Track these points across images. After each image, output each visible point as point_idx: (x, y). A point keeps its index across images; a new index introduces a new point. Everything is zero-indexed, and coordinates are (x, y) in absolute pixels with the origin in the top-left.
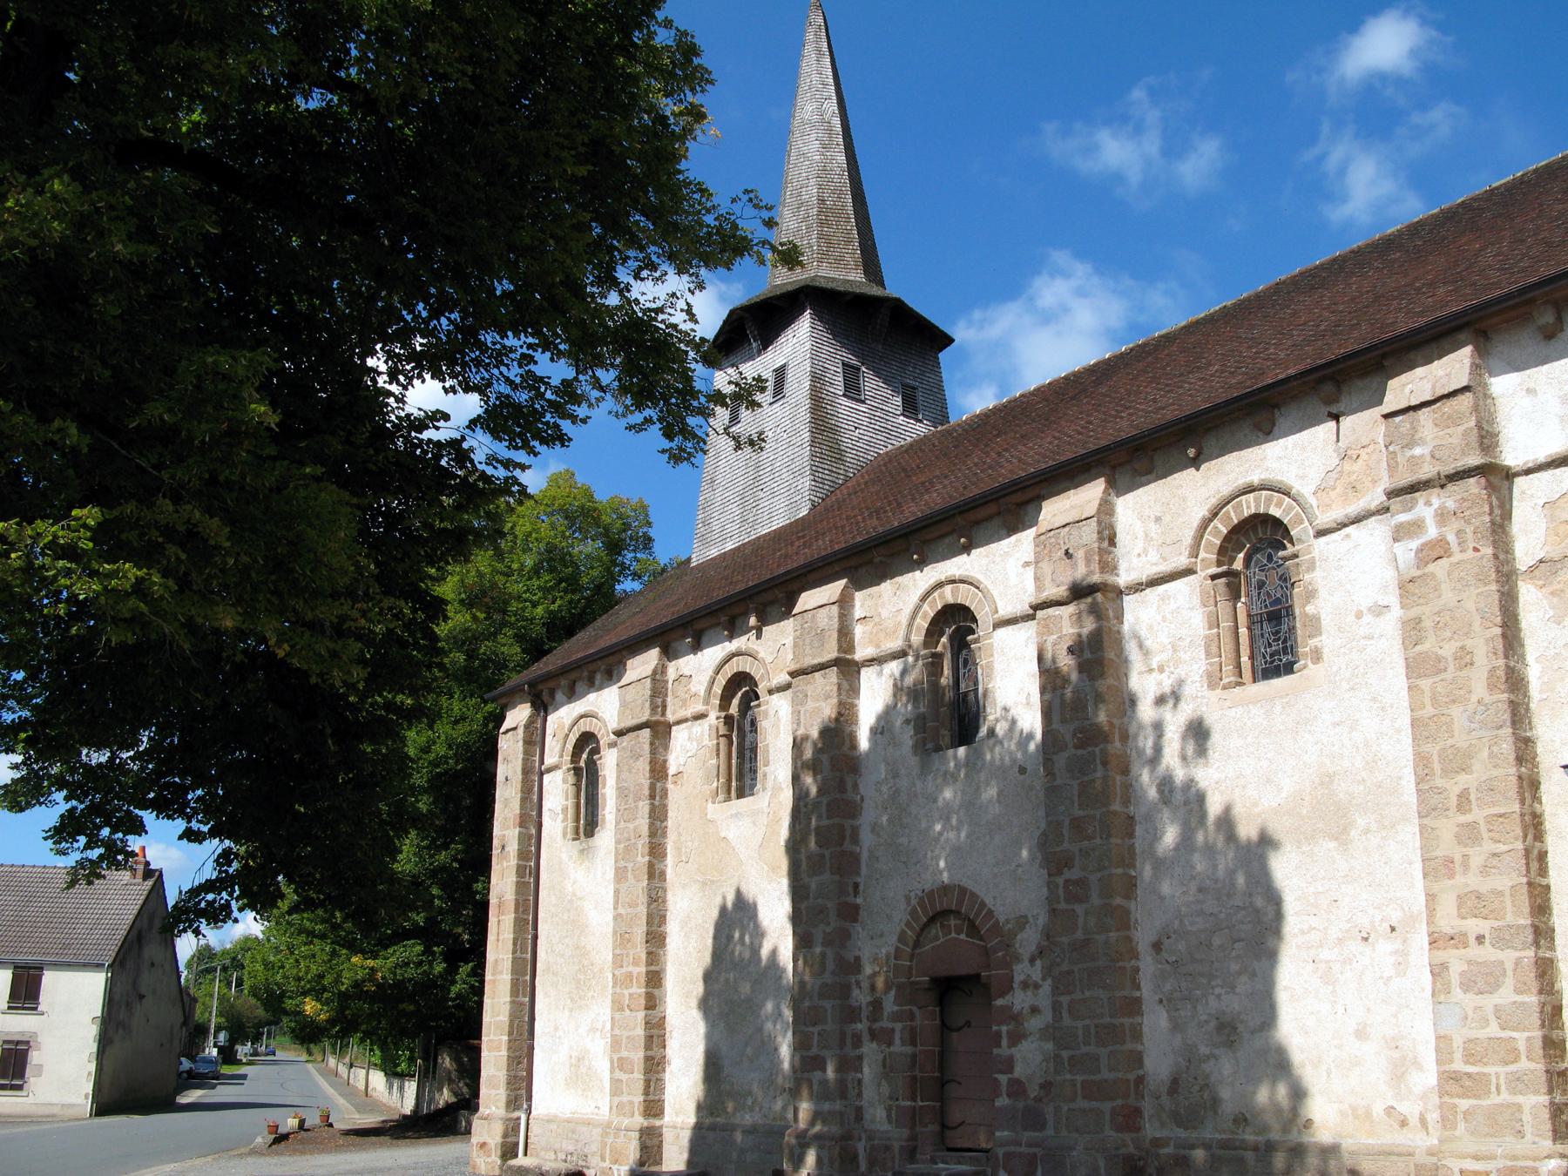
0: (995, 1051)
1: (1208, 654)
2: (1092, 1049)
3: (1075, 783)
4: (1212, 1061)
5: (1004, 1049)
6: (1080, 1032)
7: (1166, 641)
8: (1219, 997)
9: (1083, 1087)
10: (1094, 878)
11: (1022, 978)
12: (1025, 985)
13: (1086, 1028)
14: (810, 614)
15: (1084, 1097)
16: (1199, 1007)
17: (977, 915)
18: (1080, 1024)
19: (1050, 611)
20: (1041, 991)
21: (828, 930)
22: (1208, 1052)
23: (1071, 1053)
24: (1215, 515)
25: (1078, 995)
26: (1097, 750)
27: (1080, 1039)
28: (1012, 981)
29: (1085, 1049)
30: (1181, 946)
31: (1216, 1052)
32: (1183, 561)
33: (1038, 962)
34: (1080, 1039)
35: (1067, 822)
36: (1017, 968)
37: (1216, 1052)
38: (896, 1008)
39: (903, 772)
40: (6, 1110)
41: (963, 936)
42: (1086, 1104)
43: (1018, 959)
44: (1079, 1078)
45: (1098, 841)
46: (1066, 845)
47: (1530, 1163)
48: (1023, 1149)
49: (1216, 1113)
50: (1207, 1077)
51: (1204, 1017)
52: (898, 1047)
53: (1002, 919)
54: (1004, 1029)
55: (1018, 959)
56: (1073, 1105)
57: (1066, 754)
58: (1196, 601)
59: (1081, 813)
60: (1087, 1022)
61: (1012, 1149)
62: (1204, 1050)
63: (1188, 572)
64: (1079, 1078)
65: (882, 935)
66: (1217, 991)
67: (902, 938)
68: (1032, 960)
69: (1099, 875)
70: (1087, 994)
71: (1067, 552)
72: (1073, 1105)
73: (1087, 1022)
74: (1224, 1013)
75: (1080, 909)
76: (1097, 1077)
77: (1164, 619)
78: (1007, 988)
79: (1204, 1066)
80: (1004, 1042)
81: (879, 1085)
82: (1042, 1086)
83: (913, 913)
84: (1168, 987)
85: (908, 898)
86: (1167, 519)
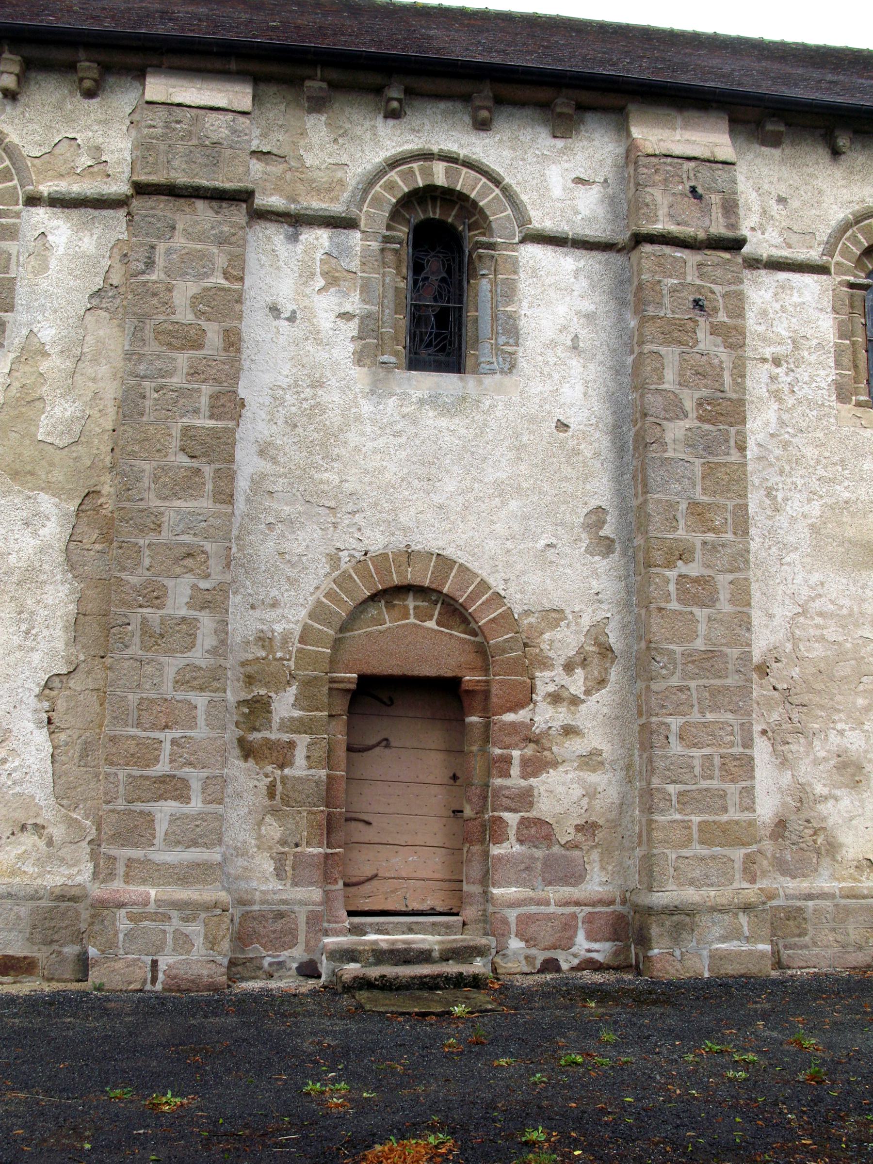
0: (498, 781)
1: (838, 364)
2: (714, 784)
3: (698, 462)
4: (830, 803)
5: (515, 780)
6: (696, 763)
7: (785, 333)
8: (841, 733)
9: (700, 831)
10: (723, 580)
11: (551, 688)
12: (555, 699)
13: (709, 758)
14: (189, 114)
15: (702, 842)
16: (816, 742)
17: (472, 598)
18: (696, 753)
19: (667, 250)
20: (583, 707)
21: (204, 584)
22: (825, 791)
23: (680, 787)
24: (857, 222)
25: (695, 717)
26: (733, 430)
27: (697, 770)
28: (532, 690)
29: (704, 784)
30: (796, 672)
31: (838, 792)
32: (814, 255)
33: (579, 672)
34: (697, 770)
35: (683, 506)
36: (542, 676)
37: (838, 792)
38: (297, 713)
39: (333, 382)
40: (11, 1001)
41: (431, 624)
42: (705, 851)
43: (545, 663)
44: (696, 819)
45: (730, 536)
46: (681, 533)
47: (799, 903)
48: (552, 909)
49: (834, 859)
50: (824, 819)
51: (822, 754)
52: (299, 768)
53: (517, 610)
54: (516, 753)
55: (545, 663)
56: (685, 852)
57: (687, 424)
58: (827, 303)
59: (706, 499)
60: (707, 751)
61: (533, 909)
62: (820, 789)
63: (822, 270)
64: (696, 819)
65: (274, 605)
66: (839, 726)
67: (318, 613)
68: (569, 668)
69: (730, 577)
70: (710, 717)
71: (693, 190)
72: (685, 852)
73: (707, 751)
74: (846, 750)
75: (700, 613)
76: (725, 818)
77: (783, 309)
78: (525, 697)
79: (821, 807)
80: (515, 771)
81: (260, 823)
82: (579, 828)
83: (343, 581)
84: (775, 716)
85: (334, 559)
86: (795, 204)
